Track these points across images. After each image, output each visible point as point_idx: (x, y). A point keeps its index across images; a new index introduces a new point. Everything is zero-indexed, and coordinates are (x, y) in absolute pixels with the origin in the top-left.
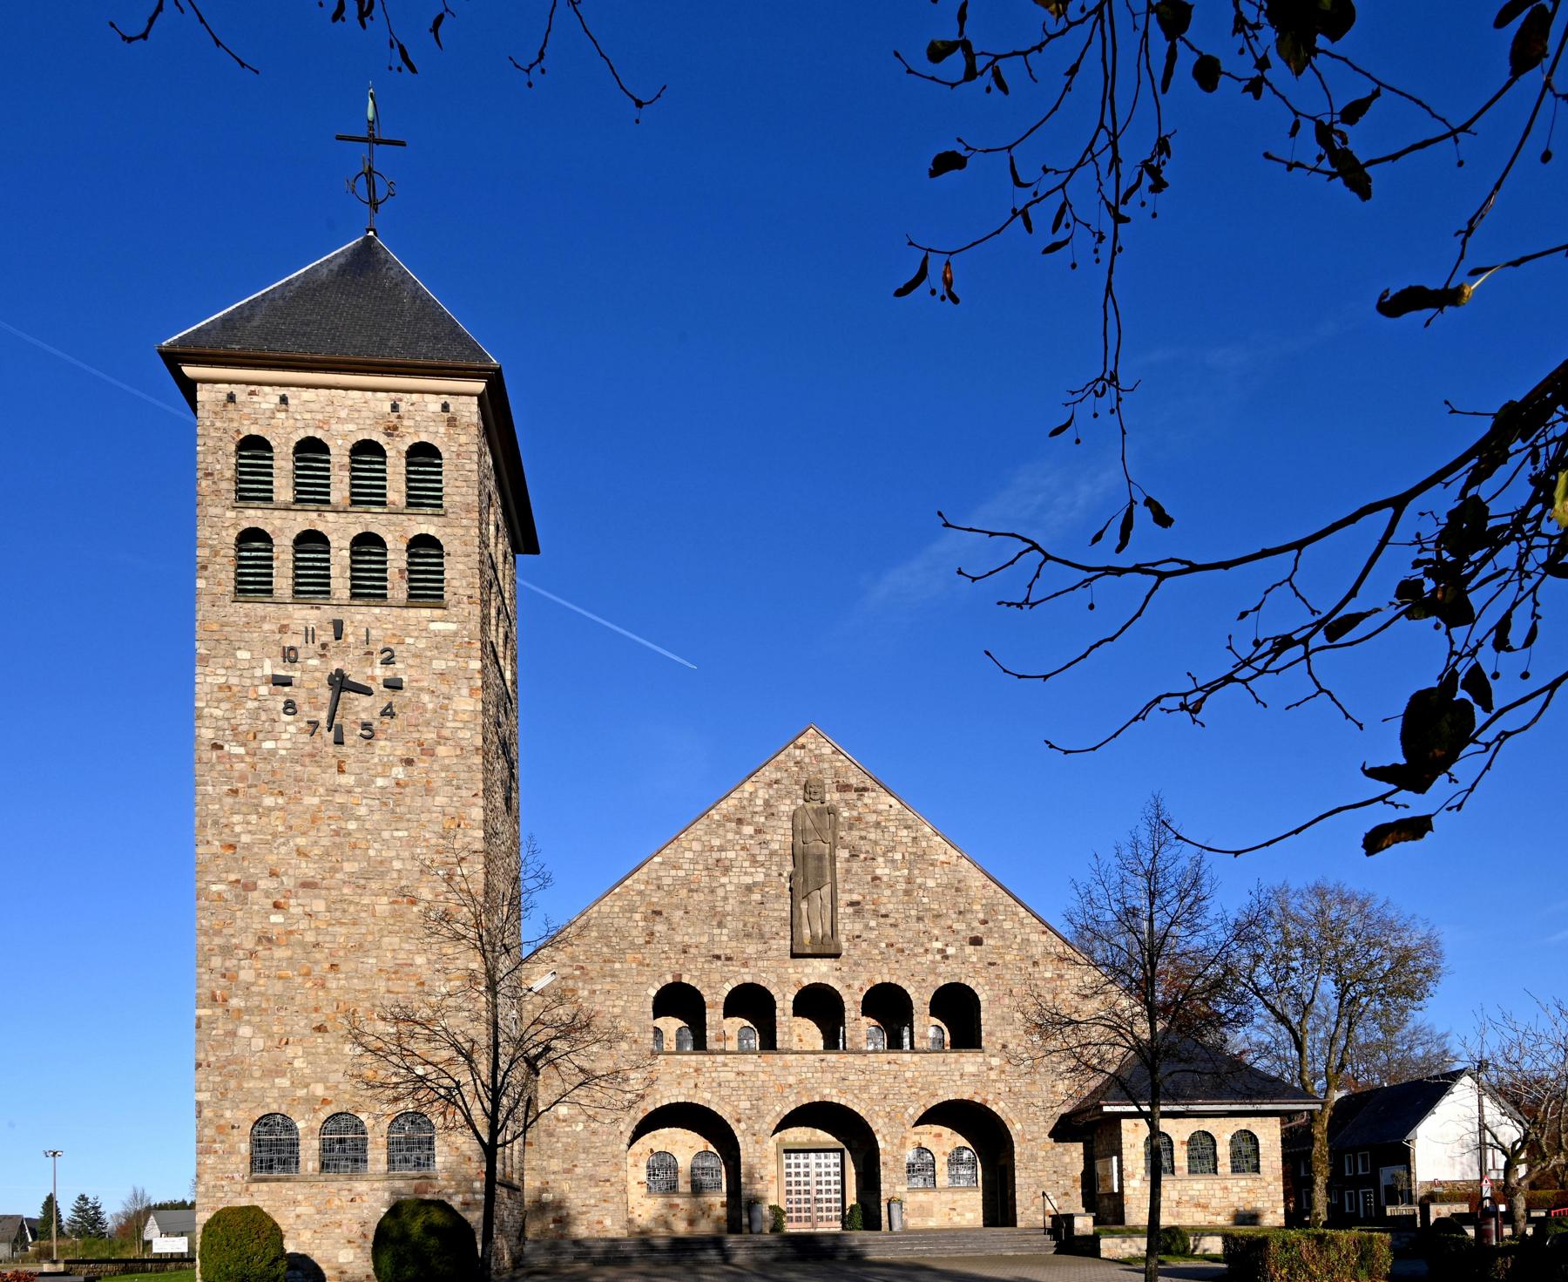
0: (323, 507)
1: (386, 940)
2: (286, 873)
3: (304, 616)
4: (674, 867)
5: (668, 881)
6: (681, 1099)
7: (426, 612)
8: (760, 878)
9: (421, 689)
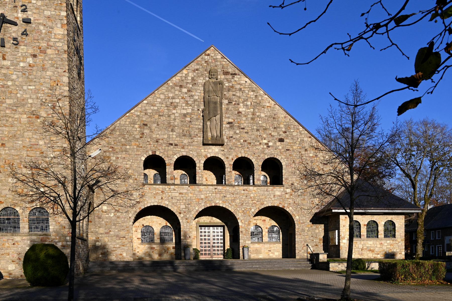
4: (153, 105)
5: (149, 111)
6: (156, 204)
8: (189, 111)
9: (39, 24)
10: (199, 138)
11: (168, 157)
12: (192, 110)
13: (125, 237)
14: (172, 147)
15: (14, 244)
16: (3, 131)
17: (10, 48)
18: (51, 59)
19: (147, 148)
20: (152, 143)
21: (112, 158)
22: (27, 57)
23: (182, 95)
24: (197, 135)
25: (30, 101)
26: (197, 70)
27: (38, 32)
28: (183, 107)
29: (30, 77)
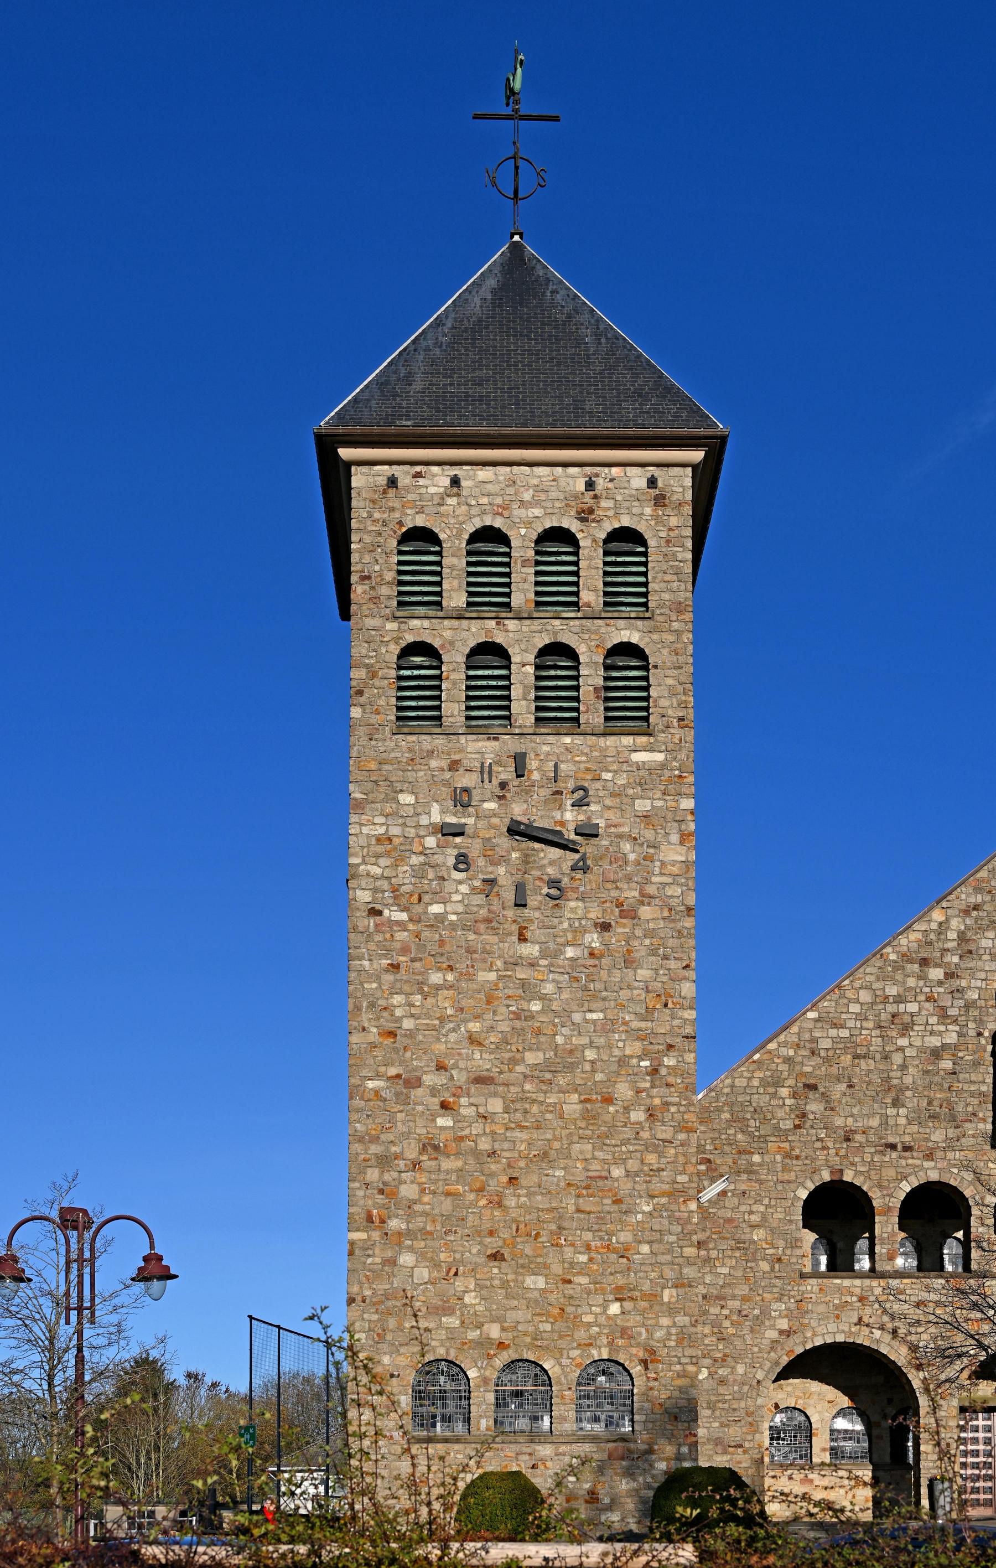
2: (456, 1066)
3: (479, 749)
4: (834, 1026)
5: (825, 1044)
6: (840, 1338)
7: (627, 740)
8: (951, 1038)
9: (620, 836)
10: (981, 1126)
12: (960, 1035)
13: (741, 1446)
14: (894, 1155)
15: (533, 1467)
16: (514, 1142)
17: (539, 908)
18: (649, 934)
19: (814, 1160)
20: (830, 1145)
23: (927, 990)
24: (974, 1115)
25: (590, 1054)
26: (976, 907)
27: (617, 860)
28: (929, 1028)
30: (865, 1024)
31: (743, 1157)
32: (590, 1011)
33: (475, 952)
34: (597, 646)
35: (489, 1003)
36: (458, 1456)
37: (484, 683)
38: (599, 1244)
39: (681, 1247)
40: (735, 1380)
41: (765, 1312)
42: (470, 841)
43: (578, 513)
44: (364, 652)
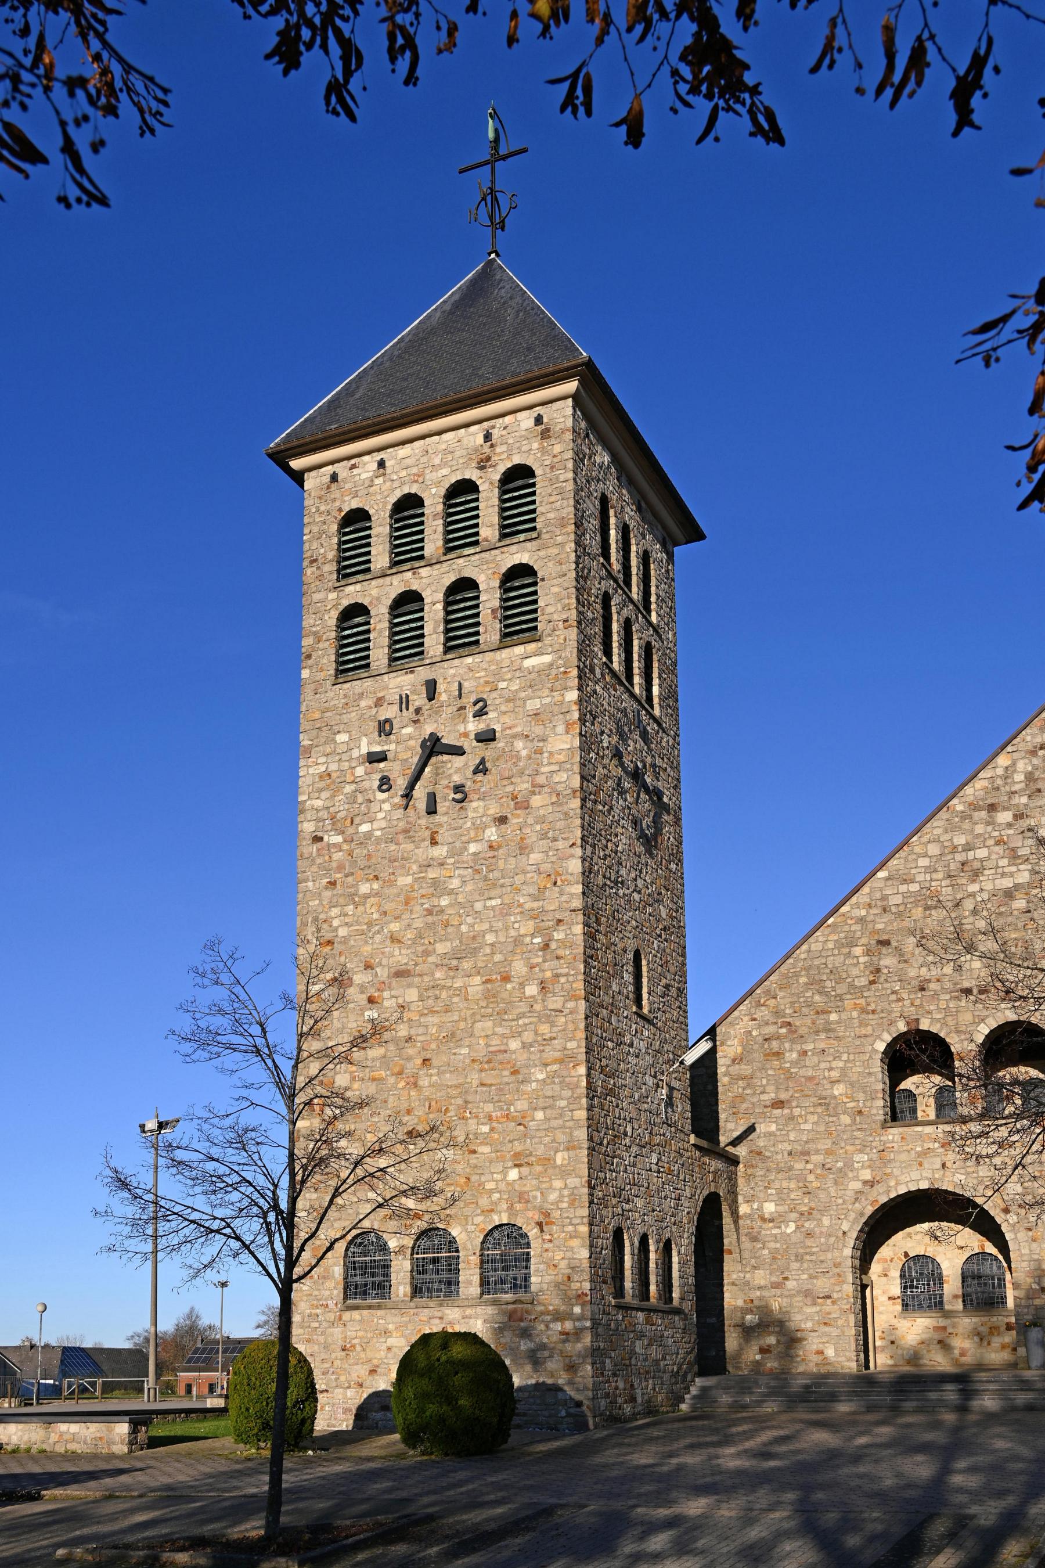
0: (416, 564)
1: (478, 1025)
2: (380, 964)
3: (406, 682)
4: (905, 881)
5: (897, 900)
6: (924, 1185)
7: (519, 650)
8: (1024, 877)
9: (515, 736)
11: (958, 1032)
13: (829, 1297)
17: (447, 813)
19: (890, 1013)
20: (905, 996)
21: (787, 1054)
22: (486, 827)
23: (996, 834)
27: (511, 757)
28: (1000, 870)
29: (491, 876)
30: (935, 876)
31: (822, 1016)
32: (490, 898)
33: (395, 860)
34: (494, 573)
35: (407, 904)
36: (380, 1321)
37: (407, 627)
38: (499, 1114)
39: (572, 1111)
40: (821, 1232)
41: (849, 1164)
42: (391, 764)
43: (479, 463)
44: (312, 622)
